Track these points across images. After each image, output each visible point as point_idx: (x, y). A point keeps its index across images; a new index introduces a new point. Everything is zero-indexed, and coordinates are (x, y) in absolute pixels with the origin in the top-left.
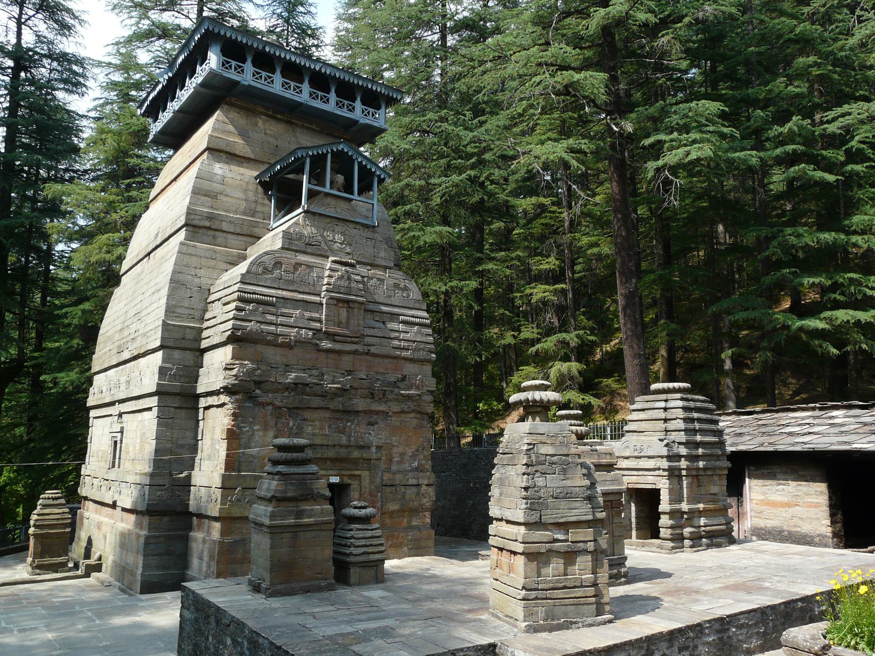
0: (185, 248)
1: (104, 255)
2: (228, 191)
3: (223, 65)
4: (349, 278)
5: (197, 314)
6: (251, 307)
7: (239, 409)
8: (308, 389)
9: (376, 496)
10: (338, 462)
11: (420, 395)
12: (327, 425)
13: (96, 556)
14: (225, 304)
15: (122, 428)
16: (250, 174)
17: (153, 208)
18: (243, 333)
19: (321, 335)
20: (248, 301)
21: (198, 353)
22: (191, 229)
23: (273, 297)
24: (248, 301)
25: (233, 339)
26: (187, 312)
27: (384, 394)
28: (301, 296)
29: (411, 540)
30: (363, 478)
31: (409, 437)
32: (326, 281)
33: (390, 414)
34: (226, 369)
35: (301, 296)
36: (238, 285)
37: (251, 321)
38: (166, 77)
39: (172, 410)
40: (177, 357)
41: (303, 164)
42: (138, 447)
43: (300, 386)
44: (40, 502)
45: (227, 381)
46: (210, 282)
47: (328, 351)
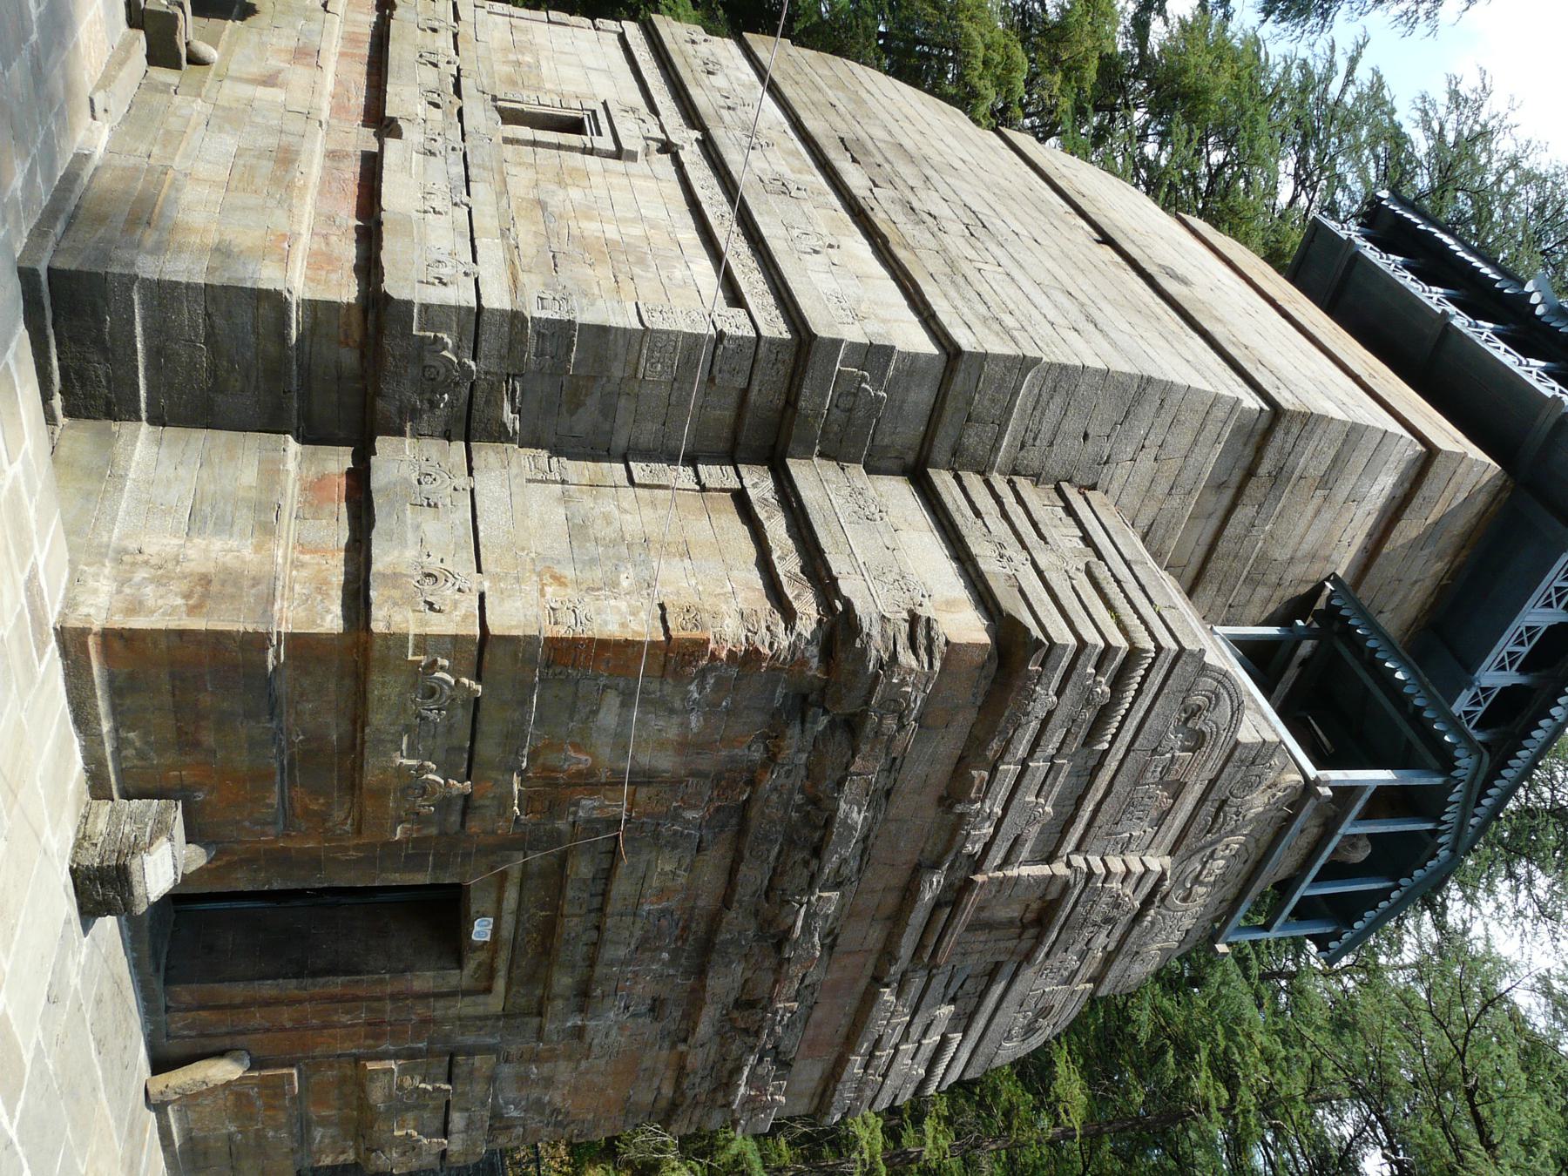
0: (1219, 413)
1: (981, 55)
2: (1327, 515)
5: (1032, 457)
7: (771, 669)
10: (540, 943)
11: (728, 1105)
12: (672, 904)
13: (204, 49)
15: (632, 156)
19: (961, 874)
20: (1118, 683)
21: (910, 458)
23: (1111, 743)
24: (1118, 683)
25: (1012, 646)
26: (1047, 428)
27: (746, 1031)
29: (260, 1135)
30: (481, 999)
32: (1117, 865)
33: (682, 1047)
34: (914, 619)
36: (1174, 647)
37: (1059, 693)
38: (1535, 299)
39: (741, 382)
42: (591, 228)
43: (817, 835)
45: (876, 632)
46: (1115, 488)
47: (909, 892)
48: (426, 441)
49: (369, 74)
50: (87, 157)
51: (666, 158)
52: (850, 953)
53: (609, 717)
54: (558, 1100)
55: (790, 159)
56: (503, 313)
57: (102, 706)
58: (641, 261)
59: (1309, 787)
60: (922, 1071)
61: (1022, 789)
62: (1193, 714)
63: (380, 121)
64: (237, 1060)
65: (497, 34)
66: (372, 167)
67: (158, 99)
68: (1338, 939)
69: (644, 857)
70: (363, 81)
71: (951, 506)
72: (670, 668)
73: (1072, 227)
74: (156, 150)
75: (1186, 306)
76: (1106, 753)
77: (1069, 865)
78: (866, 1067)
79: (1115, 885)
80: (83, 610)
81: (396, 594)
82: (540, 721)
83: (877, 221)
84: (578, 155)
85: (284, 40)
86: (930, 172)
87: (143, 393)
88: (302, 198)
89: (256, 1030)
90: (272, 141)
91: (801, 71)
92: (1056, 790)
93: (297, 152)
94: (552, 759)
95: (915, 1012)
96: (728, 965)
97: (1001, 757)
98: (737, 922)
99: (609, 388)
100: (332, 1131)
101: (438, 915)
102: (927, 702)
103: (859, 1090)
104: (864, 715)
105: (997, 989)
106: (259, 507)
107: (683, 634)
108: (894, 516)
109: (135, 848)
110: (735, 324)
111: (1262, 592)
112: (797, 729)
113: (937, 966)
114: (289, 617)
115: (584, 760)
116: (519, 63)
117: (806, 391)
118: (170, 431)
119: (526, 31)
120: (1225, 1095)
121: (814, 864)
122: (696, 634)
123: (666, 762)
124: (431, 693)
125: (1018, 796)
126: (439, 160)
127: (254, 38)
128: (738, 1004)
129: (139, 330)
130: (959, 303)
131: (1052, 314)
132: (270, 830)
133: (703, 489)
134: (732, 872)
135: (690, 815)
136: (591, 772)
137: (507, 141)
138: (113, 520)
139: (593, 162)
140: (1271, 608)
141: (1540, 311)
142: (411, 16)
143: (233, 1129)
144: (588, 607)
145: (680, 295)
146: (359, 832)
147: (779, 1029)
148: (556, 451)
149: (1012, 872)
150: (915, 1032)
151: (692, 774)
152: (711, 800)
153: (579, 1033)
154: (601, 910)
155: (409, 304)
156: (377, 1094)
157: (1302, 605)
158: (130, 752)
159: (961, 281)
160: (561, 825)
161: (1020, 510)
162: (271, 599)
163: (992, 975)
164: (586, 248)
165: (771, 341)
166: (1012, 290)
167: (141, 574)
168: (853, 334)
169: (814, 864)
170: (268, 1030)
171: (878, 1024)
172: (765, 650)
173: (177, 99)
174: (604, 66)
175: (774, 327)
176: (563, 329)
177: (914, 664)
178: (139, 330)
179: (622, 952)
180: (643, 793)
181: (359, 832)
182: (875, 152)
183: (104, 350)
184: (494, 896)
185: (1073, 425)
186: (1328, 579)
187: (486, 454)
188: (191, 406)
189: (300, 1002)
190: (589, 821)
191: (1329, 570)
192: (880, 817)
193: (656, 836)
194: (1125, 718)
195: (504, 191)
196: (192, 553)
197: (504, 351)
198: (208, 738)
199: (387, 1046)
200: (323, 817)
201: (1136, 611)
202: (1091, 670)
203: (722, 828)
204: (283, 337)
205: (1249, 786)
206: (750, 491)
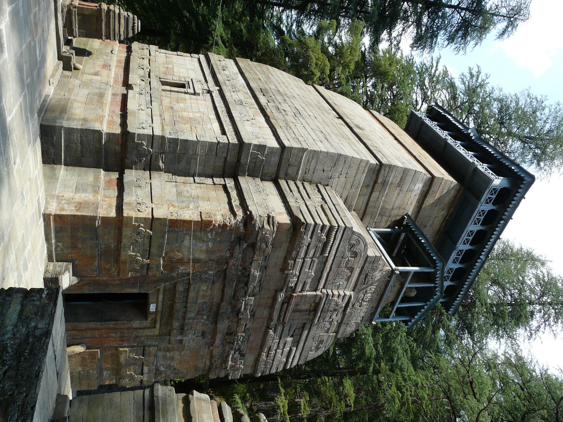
0: (363, 164)
1: (314, 62)
2: (402, 195)
3: (494, 189)
4: (335, 310)
5: (308, 176)
6: (324, 237)
7: (230, 230)
8: (242, 285)
9: (134, 342)
10: (169, 311)
11: (226, 368)
12: (206, 300)
13: (78, 65)
14: (322, 206)
15: (199, 94)
16: (410, 210)
17: (365, 113)
18: (301, 233)
19: (289, 293)
20: (328, 235)
21: (274, 176)
22: (377, 168)
23: (329, 254)
24: (328, 235)
25: (296, 224)
26: (312, 168)
27: (230, 343)
28: (325, 274)
30: (152, 330)
31: (188, 362)
32: (336, 292)
33: (211, 348)
34: (269, 217)
35: (325, 274)
36: (343, 226)
37: (311, 238)
39: (224, 155)
40: (273, 159)
41: (428, 266)
42: (185, 114)
43: (246, 279)
44: (131, 15)
45: (258, 219)
46: (334, 185)
48: (139, 171)
49: (124, 71)
50: (49, 96)
51: (209, 95)
52: (259, 318)
53: (186, 243)
54: (175, 365)
55: (245, 95)
56: (159, 136)
57: (53, 235)
58: (199, 123)
59: (393, 271)
60: (285, 360)
61: (304, 267)
62: (353, 246)
63: (127, 85)
64: (83, 346)
65: (161, 59)
66: (125, 98)
67: (66, 80)
68: (411, 322)
69: (198, 285)
70: (122, 74)
71: (283, 189)
72: (203, 228)
73: (329, 114)
74: (66, 94)
75: (360, 136)
76: (328, 257)
77: (321, 292)
78: (267, 357)
79: (336, 298)
80: (49, 210)
81: (130, 207)
82: (167, 244)
83: (267, 112)
84: (183, 94)
85: (100, 62)
86: (286, 98)
87: (63, 157)
88: (106, 106)
89: (88, 338)
90: (97, 91)
91: (252, 69)
92: (314, 268)
93: (104, 94)
94: (172, 255)
95: (280, 339)
96: (223, 321)
97: (297, 257)
98: (226, 307)
99: (189, 157)
100: (109, 372)
101: (139, 303)
102: (274, 239)
103: (265, 365)
104: (256, 243)
105: (306, 332)
106: (93, 186)
107: (206, 219)
108: (268, 191)
109: (60, 273)
110: (223, 139)
111: (385, 218)
112: (238, 247)
113: (285, 323)
114: (102, 213)
115: (180, 255)
116: (167, 68)
117: (242, 158)
118: (70, 168)
119: (170, 58)
120: (400, 395)
121: (246, 288)
122: (209, 219)
123: (203, 256)
124: (139, 234)
125: (303, 269)
126: (143, 96)
127: (92, 62)
128: (227, 334)
129: (63, 140)
130: (287, 134)
131: (315, 137)
132: (95, 273)
133: (215, 184)
134: (223, 291)
135: (210, 272)
136: (182, 259)
137: (163, 90)
138: (56, 189)
139: (187, 96)
140: (388, 223)
141: (473, 138)
142: (136, 54)
143: (81, 369)
144: (181, 212)
145: (210, 132)
146: (119, 274)
147: (240, 342)
148: (174, 174)
149: (305, 293)
150: (281, 346)
151: (210, 260)
152: (216, 268)
153: (181, 341)
154: (186, 302)
155: (134, 134)
156: (122, 359)
157: (399, 222)
158: (59, 249)
159: (289, 128)
160: (174, 274)
161: (304, 191)
162: (97, 208)
163: (303, 328)
164: (184, 119)
165: (233, 144)
166: (304, 131)
167: (63, 202)
168: (255, 142)
169: (246, 288)
170: (92, 338)
171: (269, 342)
172: (228, 224)
173: (71, 80)
174: (193, 68)
175: (233, 140)
176: (175, 141)
177: (269, 228)
178: (63, 140)
179: (192, 315)
180: (197, 265)
181: (119, 274)
182: (270, 92)
183: (54, 146)
184: (156, 297)
185: (319, 167)
186: (406, 215)
187: (155, 174)
188: (76, 161)
189: (101, 329)
190: (182, 273)
191: (406, 212)
192: (264, 275)
193: (201, 278)
194: (332, 246)
195: (161, 104)
196: (76, 197)
197: (160, 147)
198: (80, 245)
199: (125, 344)
200: (109, 270)
201: (334, 216)
202: (319, 232)
203: (220, 276)
204: (101, 142)
205: (374, 270)
206: (227, 185)
